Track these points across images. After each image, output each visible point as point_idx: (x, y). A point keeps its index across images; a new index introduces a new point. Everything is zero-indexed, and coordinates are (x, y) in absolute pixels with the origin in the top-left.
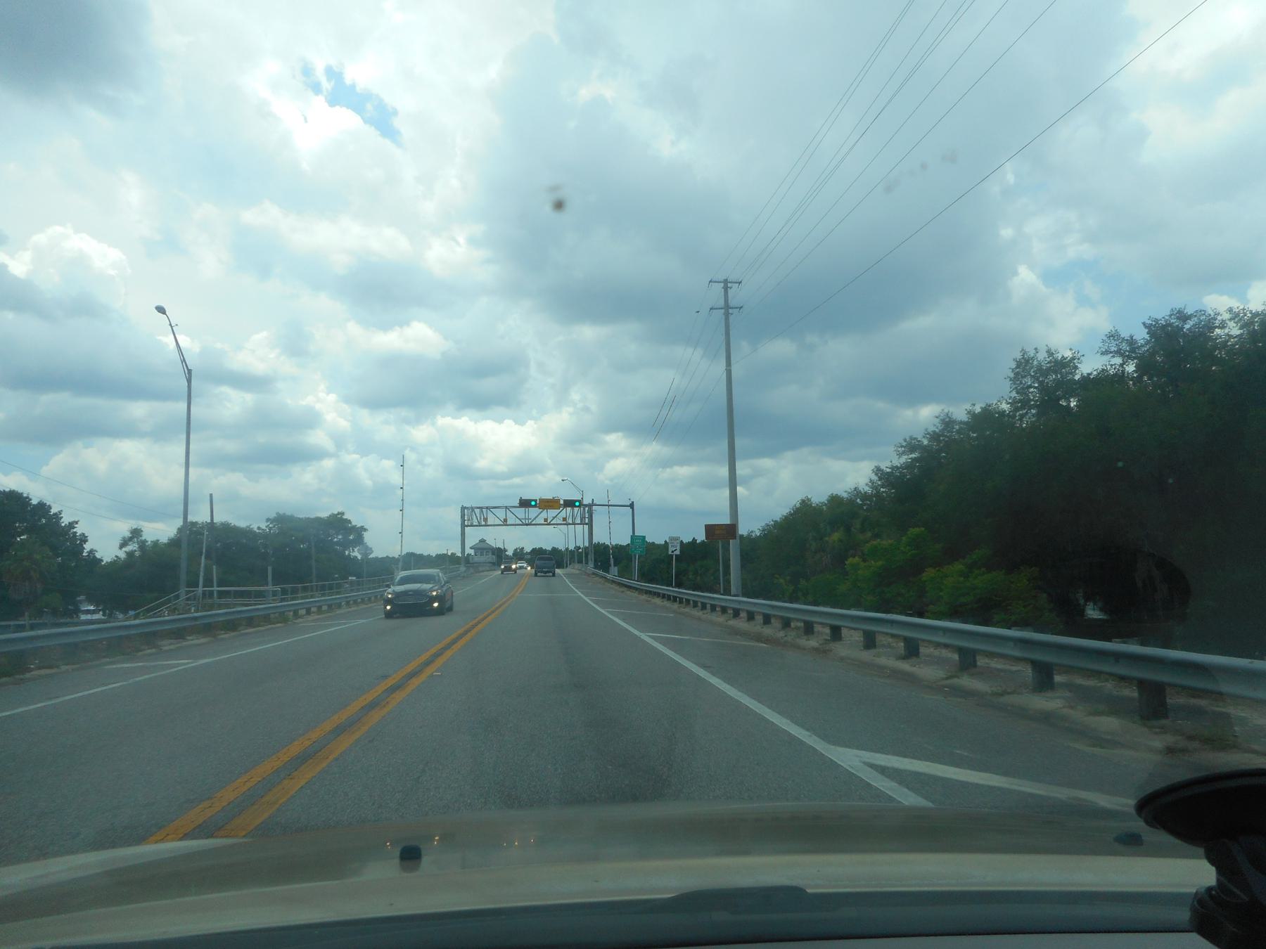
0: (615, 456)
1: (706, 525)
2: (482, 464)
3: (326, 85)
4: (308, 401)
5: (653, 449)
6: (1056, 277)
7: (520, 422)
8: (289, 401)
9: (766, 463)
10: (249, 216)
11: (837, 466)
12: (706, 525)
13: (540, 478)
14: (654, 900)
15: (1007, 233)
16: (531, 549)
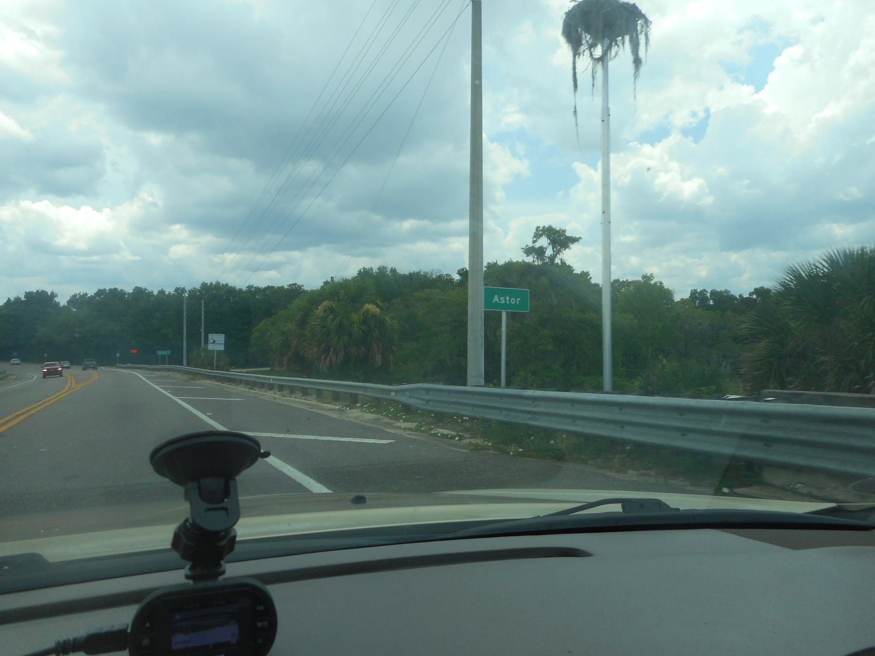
0: (179, 242)
1: (26, 293)
2: (62, 242)
5: (208, 239)
7: (99, 209)
9: (295, 254)
12: (26, 293)
13: (116, 257)
14: (355, 530)
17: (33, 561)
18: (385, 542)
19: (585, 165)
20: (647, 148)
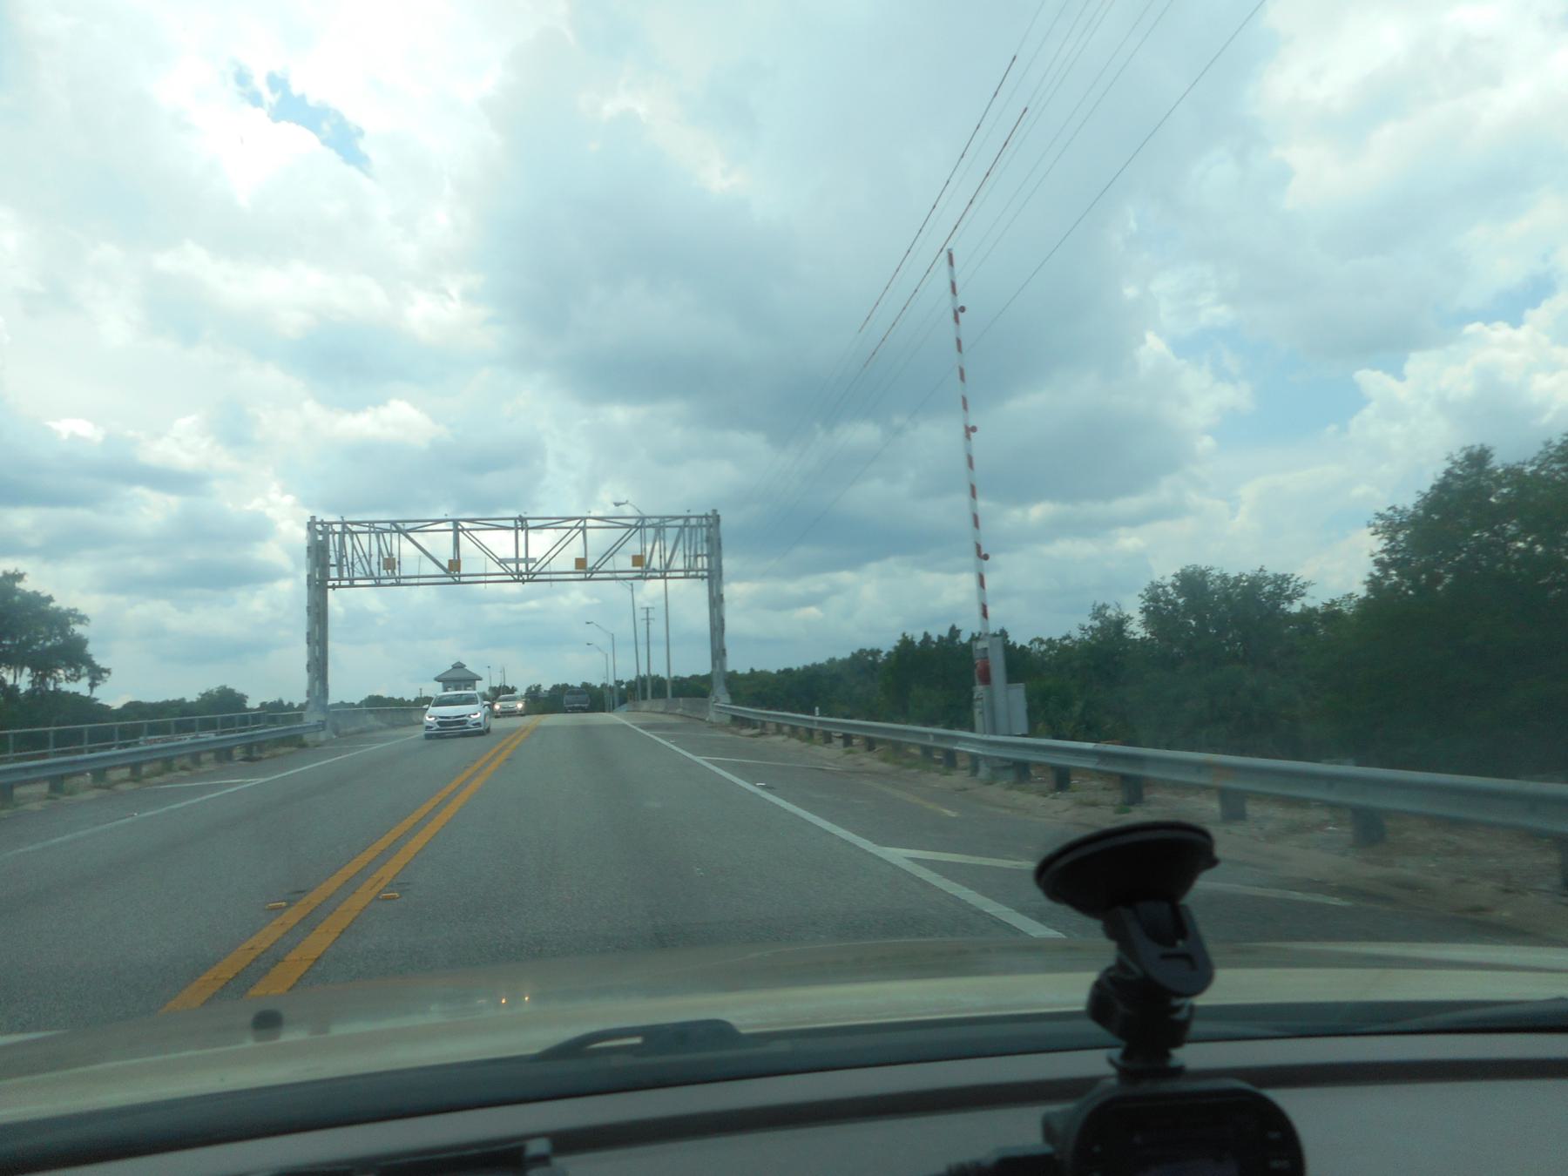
3: (270, 98)
4: (256, 504)
6: (1188, 347)
8: (229, 505)
9: (845, 577)
10: (165, 262)
11: (929, 579)
15: (1130, 292)
16: (551, 686)
17: (719, 1032)
18: (1276, 1033)
19: (1378, 374)
20: (1501, 331)
